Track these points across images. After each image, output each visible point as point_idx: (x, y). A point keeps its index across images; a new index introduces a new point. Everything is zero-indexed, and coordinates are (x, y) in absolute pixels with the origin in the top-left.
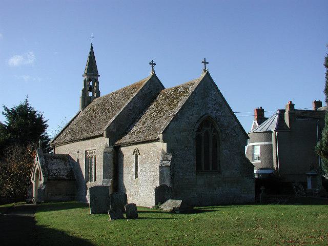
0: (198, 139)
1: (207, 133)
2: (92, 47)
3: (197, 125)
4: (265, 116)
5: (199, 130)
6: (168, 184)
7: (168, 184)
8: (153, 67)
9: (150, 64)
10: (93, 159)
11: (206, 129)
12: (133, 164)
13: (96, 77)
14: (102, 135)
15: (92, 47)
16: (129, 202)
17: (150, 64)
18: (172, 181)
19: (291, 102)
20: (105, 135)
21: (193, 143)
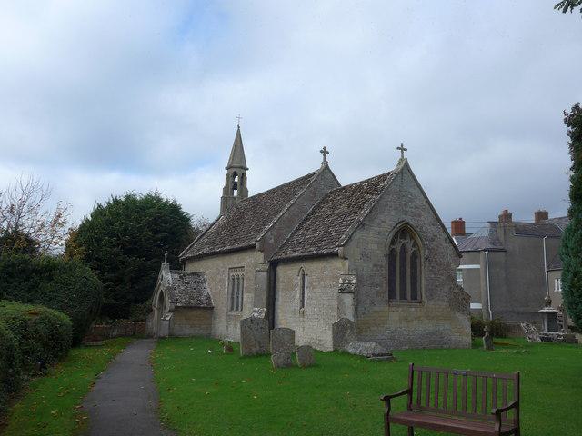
0: (391, 256)
1: (403, 247)
2: (239, 131)
3: (391, 235)
4: (466, 231)
5: (393, 243)
6: (350, 316)
7: (350, 316)
8: (324, 155)
9: (321, 151)
10: (236, 280)
11: (403, 241)
12: (298, 290)
13: (243, 171)
14: (252, 247)
15: (239, 131)
16: (498, 220)
17: (321, 151)
18: (356, 315)
19: (506, 211)
20: (398, 321)
21: (384, 262)
